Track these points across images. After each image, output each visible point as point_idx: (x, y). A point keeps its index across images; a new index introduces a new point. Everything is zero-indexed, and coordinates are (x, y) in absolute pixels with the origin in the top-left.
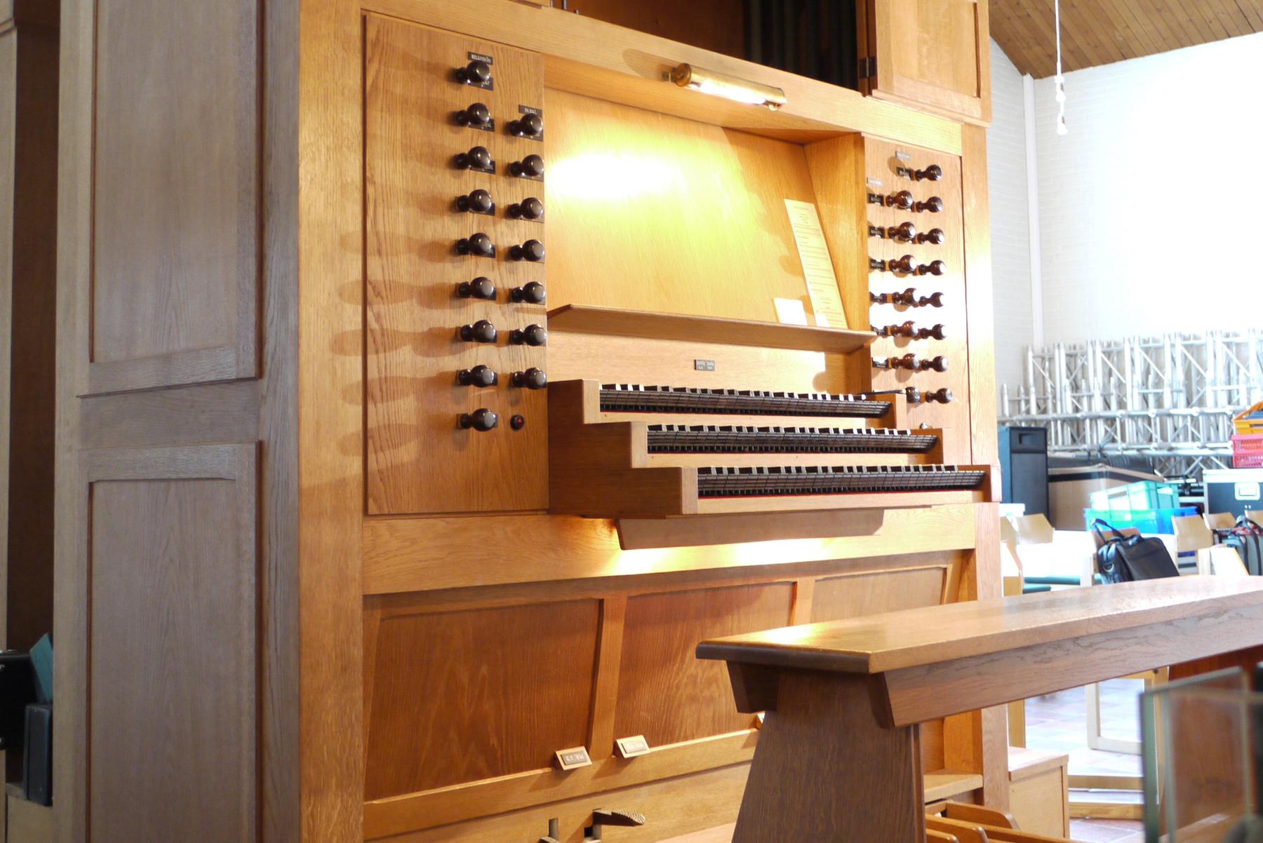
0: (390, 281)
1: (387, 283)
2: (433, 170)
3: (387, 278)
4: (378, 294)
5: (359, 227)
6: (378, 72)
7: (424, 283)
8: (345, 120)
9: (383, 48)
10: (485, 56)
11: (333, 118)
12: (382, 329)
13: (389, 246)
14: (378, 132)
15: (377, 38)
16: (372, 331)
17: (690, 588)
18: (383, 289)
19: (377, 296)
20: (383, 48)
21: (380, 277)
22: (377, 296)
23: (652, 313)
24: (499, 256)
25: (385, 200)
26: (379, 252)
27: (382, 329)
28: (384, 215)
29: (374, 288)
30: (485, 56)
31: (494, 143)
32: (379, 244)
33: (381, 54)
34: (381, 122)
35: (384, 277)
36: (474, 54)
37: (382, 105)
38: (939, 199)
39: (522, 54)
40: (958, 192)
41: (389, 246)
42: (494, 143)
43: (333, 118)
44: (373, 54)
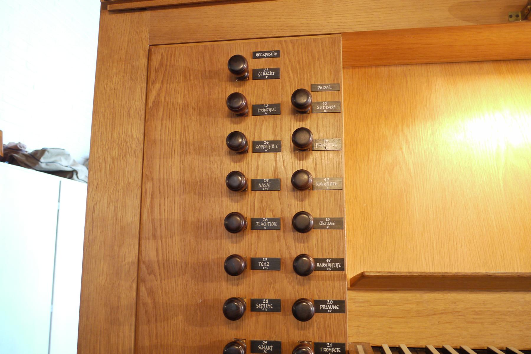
0: (163, 260)
1: (161, 262)
2: (212, 159)
3: (161, 259)
4: (151, 272)
5: (137, 219)
6: (160, 89)
7: (259, 103)
8: (129, 133)
9: (166, 70)
10: (270, 52)
11: (119, 134)
12: (154, 302)
13: (163, 230)
14: (158, 137)
15: (161, 64)
16: (144, 304)
17: (162, 302)
18: (157, 268)
19: (150, 274)
20: (166, 70)
21: (154, 258)
22: (150, 274)
23: (397, 293)
24: (285, 226)
25: (162, 192)
26: (154, 236)
27: (154, 302)
28: (160, 205)
29: (148, 268)
30: (270, 52)
31: (281, 124)
32: (154, 229)
33: (164, 75)
34: (161, 129)
35: (157, 255)
36: (258, 52)
37: (163, 115)
38: (364, 272)
39: (315, 40)
40: (131, 325)
41: (163, 230)
42: (281, 124)
43: (119, 134)
44: (156, 77)
